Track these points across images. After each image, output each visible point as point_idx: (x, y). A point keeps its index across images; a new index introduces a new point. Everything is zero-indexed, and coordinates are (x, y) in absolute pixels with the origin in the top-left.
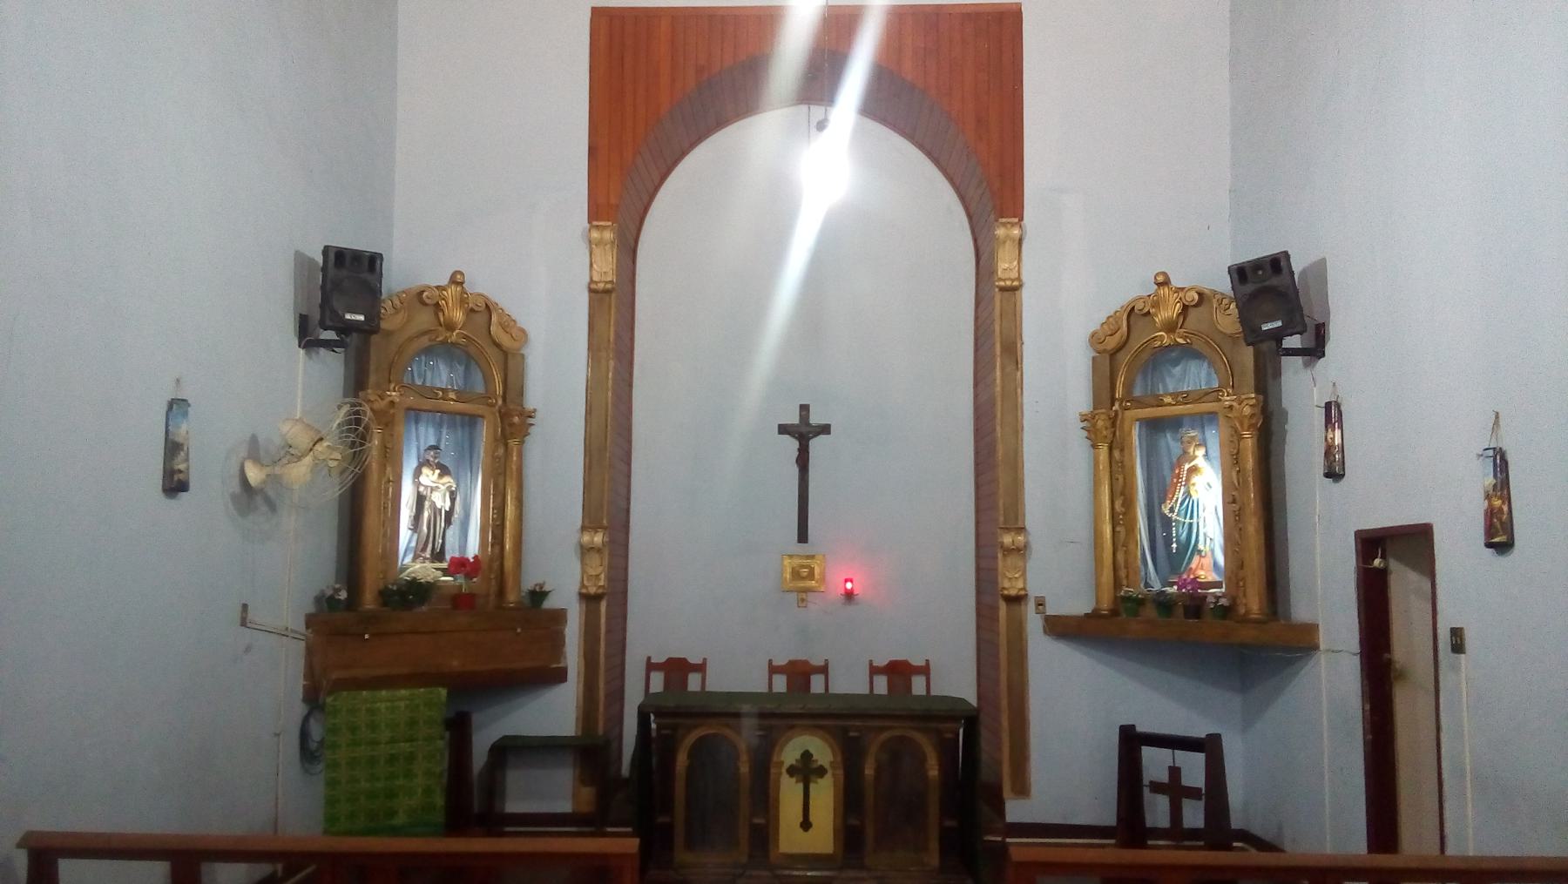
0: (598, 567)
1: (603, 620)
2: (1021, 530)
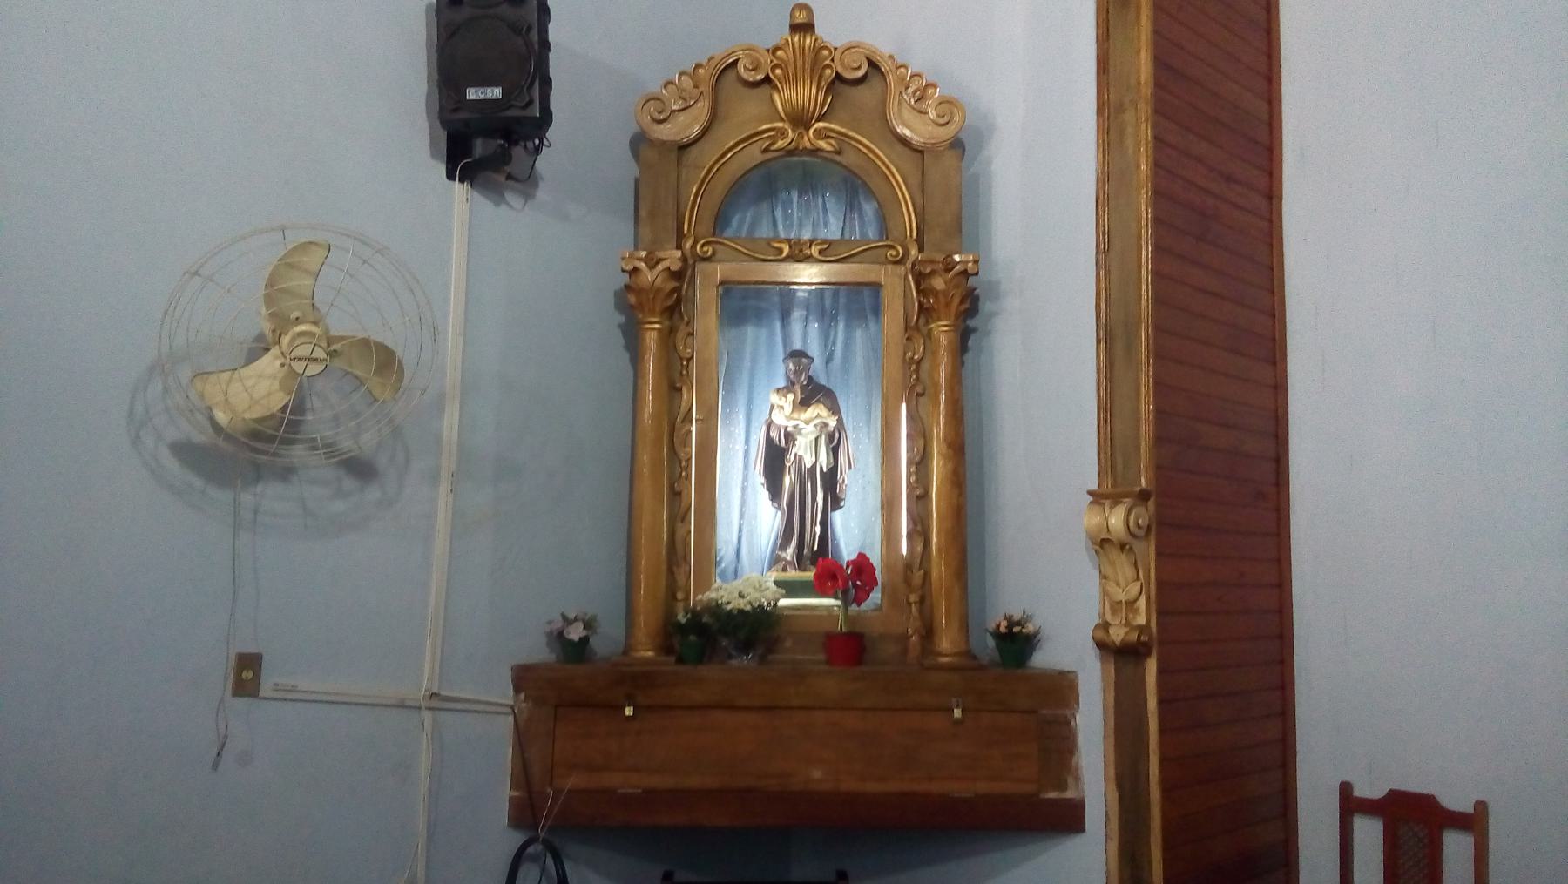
1: (1152, 704)
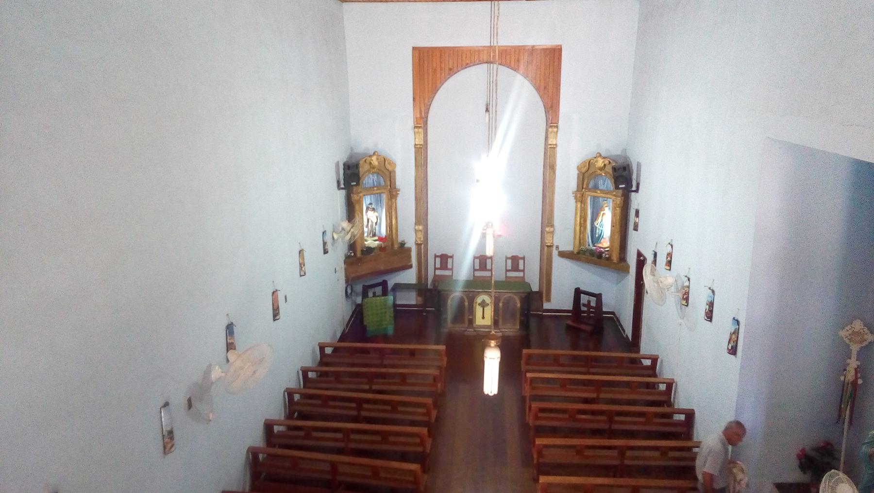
0: (421, 235)
2: (552, 226)
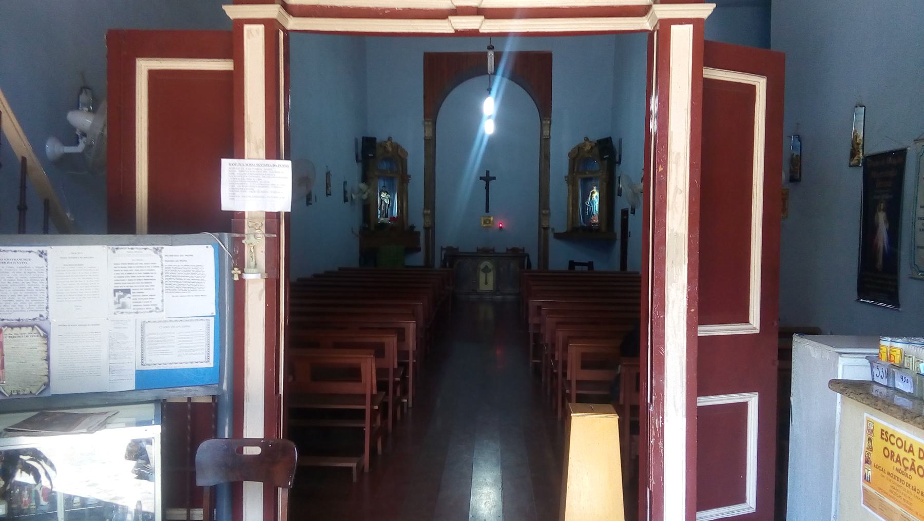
2: (548, 209)
